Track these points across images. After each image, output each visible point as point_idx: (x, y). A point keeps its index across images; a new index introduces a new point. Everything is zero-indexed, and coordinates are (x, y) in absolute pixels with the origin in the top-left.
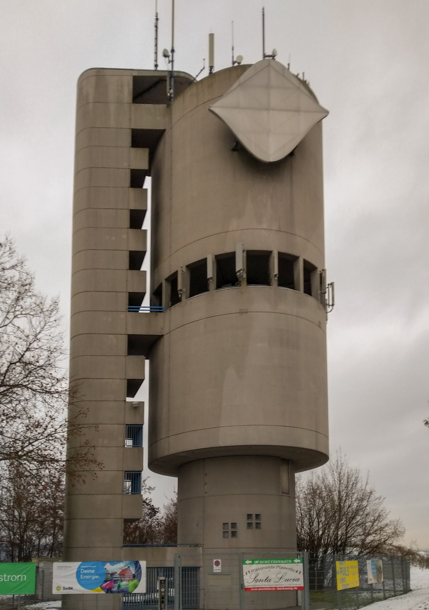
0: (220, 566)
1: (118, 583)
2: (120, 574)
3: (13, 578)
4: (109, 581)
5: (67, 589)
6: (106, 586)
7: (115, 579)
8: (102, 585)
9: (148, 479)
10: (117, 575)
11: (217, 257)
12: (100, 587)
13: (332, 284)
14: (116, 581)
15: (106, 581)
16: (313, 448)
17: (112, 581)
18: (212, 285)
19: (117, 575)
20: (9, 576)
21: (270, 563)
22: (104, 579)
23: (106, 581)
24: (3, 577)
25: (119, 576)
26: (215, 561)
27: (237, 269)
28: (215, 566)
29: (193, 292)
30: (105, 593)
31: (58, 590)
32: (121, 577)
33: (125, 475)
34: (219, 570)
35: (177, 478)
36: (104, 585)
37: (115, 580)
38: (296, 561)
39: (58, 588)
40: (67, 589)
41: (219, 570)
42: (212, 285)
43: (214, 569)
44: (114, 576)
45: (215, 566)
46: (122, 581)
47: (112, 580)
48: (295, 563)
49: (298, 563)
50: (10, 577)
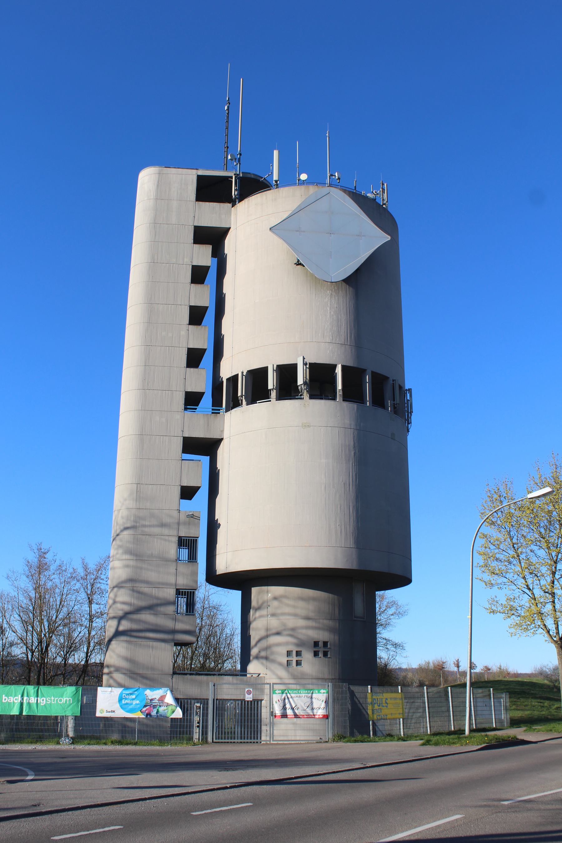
0: (251, 695)
1: (157, 708)
2: (159, 700)
3: (60, 701)
4: (149, 705)
5: (109, 712)
6: (146, 710)
7: (154, 704)
8: (142, 709)
9: (109, 710)
10: (156, 701)
11: (277, 365)
12: (140, 711)
13: (410, 390)
14: (155, 707)
15: (145, 706)
16: (385, 569)
17: (152, 706)
18: (273, 394)
19: (156, 701)
20: (56, 699)
21: (298, 693)
22: (144, 704)
23: (145, 706)
24: (51, 700)
25: (158, 702)
26: (246, 690)
27: (299, 383)
28: (246, 695)
29: (252, 401)
30: (145, 717)
31: (101, 713)
32: (160, 703)
33: (87, 757)
34: (251, 698)
35: (241, 592)
36: (144, 709)
37: (154, 706)
38: (322, 691)
39: (102, 711)
40: (109, 712)
41: (251, 698)
42: (273, 394)
43: (246, 697)
44: (153, 702)
45: (246, 695)
46: (160, 706)
47: (151, 705)
48: (321, 693)
49: (279, 693)
50: (57, 700)
